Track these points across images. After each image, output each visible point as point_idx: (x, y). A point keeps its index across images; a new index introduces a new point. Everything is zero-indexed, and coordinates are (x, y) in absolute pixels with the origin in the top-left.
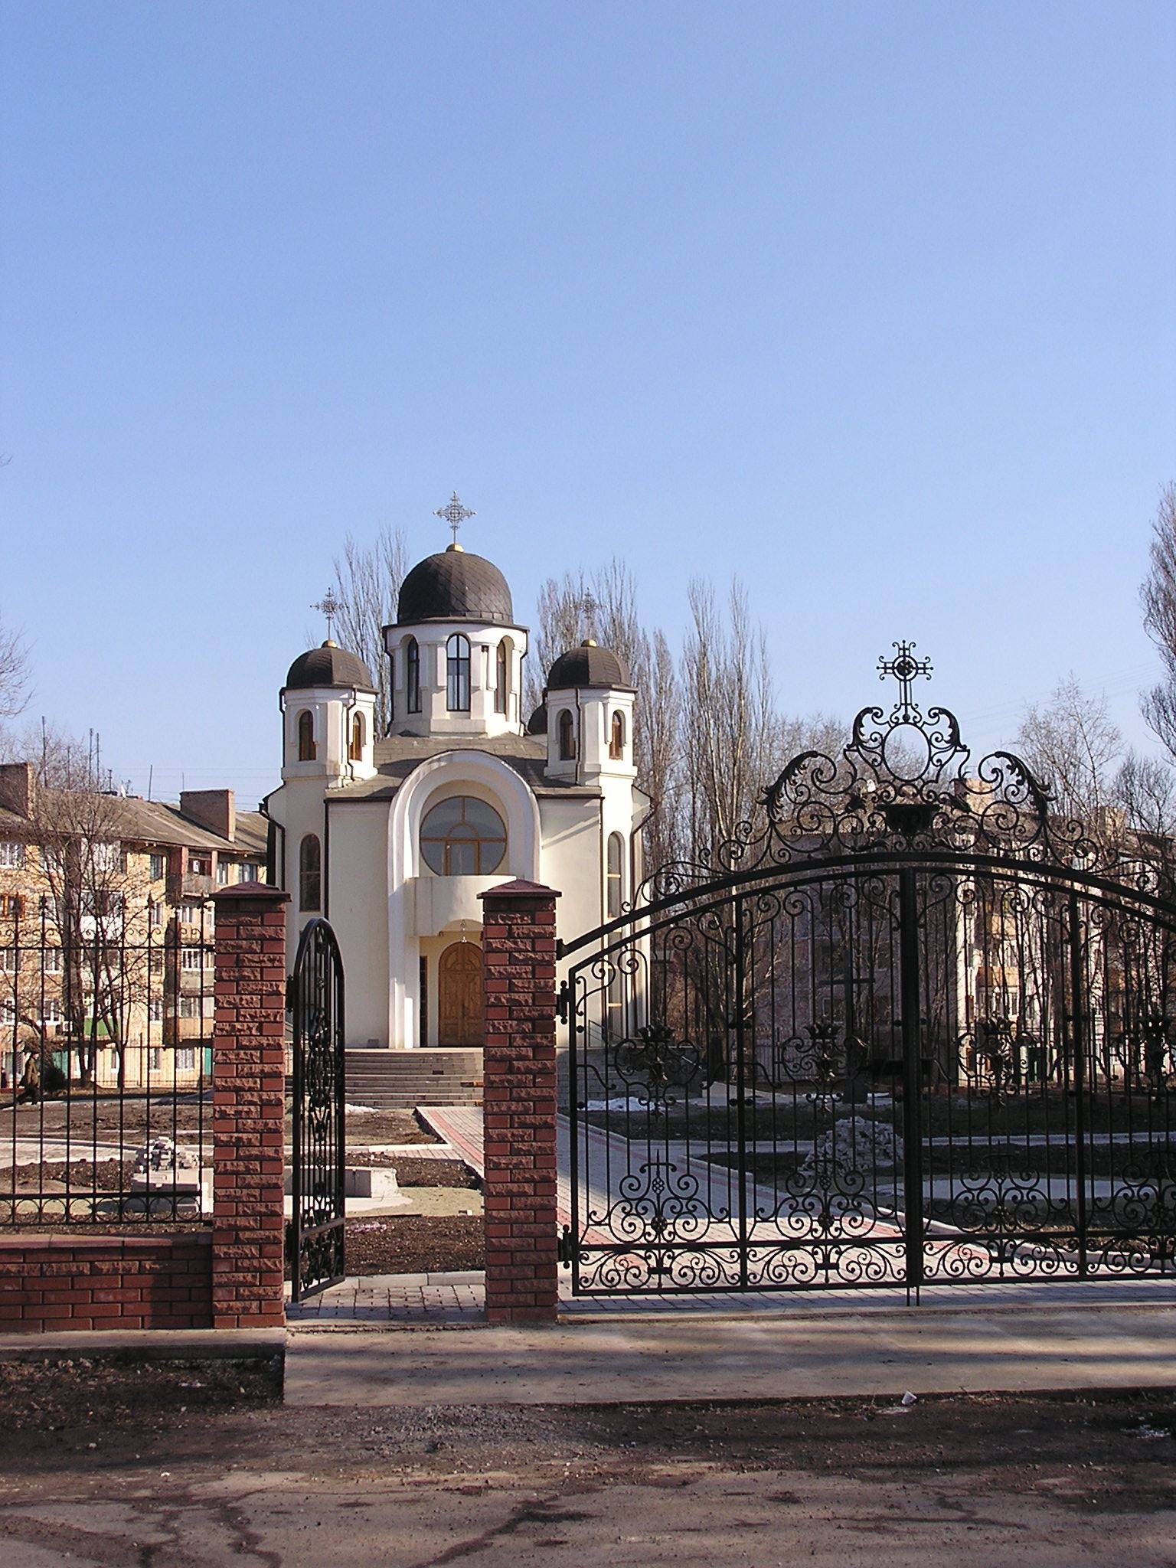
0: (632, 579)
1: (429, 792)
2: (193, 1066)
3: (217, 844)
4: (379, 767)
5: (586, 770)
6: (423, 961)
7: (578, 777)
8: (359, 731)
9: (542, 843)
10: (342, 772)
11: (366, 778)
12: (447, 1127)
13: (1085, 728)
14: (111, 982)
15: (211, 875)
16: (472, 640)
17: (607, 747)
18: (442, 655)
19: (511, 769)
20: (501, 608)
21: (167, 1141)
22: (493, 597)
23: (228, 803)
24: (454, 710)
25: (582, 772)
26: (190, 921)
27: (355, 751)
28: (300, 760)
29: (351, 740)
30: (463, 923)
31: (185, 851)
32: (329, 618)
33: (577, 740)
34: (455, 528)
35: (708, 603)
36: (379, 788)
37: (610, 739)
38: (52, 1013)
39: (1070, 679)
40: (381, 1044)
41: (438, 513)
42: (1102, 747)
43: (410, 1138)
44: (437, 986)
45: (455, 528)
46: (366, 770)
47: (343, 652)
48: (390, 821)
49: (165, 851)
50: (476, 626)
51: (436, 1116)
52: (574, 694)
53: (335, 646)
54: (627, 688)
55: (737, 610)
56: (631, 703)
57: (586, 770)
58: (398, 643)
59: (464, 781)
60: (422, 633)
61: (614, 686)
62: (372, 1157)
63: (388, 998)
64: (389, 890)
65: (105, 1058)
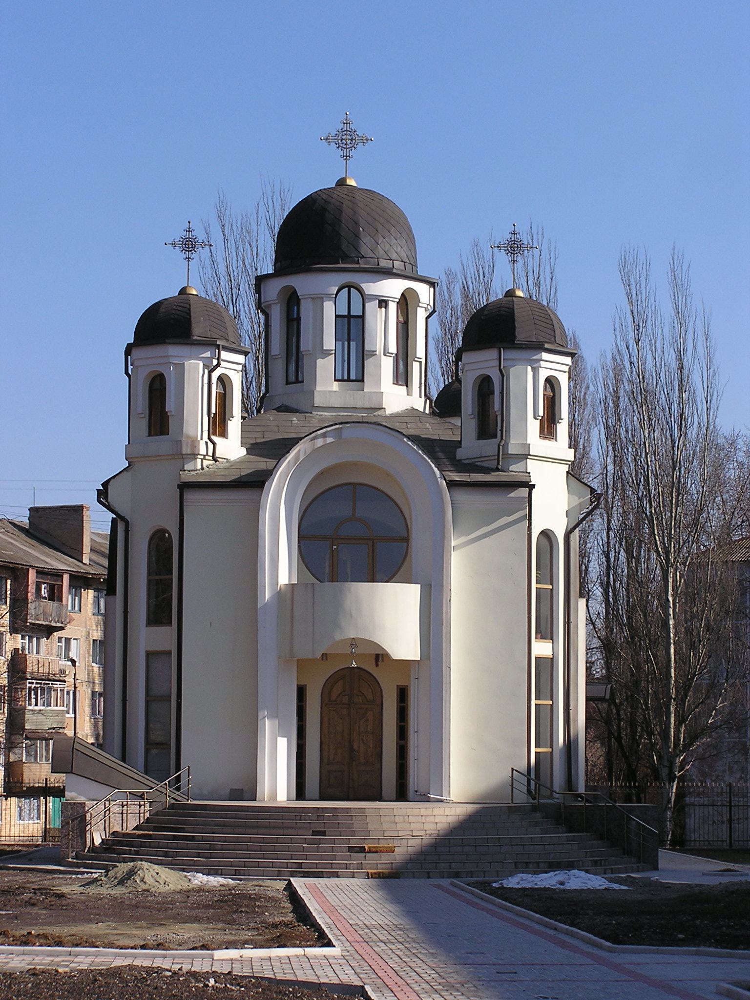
0: (552, 249)
3: (69, 565)
4: (248, 446)
6: (301, 692)
8: (224, 400)
10: (203, 451)
12: (331, 911)
18: (329, 310)
20: (403, 255)
25: (506, 455)
26: (38, 653)
27: (218, 425)
28: (150, 435)
29: (213, 410)
30: (354, 643)
34: (346, 157)
35: (643, 279)
45: (346, 157)
47: (210, 308)
51: (317, 893)
53: (194, 293)
55: (678, 287)
60: (304, 284)
61: (546, 346)
62: (212, 982)
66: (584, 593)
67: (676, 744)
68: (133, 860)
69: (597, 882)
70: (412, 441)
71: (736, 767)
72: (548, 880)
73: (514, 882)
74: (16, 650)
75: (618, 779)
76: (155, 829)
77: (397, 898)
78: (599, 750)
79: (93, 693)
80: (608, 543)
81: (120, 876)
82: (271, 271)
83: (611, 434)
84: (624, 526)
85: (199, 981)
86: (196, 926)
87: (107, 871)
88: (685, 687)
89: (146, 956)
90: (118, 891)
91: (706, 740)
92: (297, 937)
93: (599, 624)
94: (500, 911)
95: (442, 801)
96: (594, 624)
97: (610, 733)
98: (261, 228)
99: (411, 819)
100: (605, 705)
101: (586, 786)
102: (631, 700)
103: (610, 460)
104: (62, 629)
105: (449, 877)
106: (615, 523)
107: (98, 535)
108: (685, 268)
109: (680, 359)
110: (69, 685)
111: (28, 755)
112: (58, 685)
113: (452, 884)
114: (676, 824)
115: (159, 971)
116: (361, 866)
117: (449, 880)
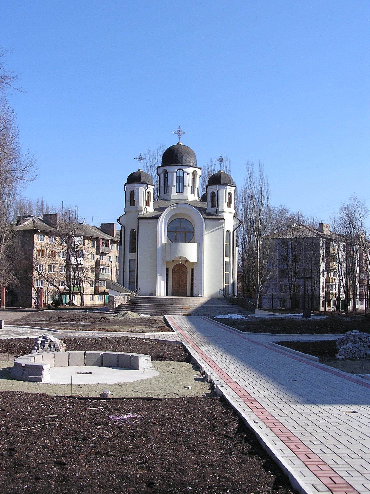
1: (169, 218)
2: (103, 300)
5: (219, 211)
6: (167, 269)
7: (217, 212)
8: (149, 197)
9: (205, 233)
10: (143, 210)
11: (151, 212)
12: (174, 323)
13: (359, 209)
14: (79, 275)
15: (108, 246)
16: (184, 171)
17: (226, 203)
18: (175, 175)
19: (196, 209)
21: (48, 335)
22: (191, 158)
23: (114, 227)
24: (178, 193)
25: (218, 211)
26: (103, 259)
27: (147, 203)
28: (130, 206)
29: (146, 200)
30: (180, 257)
32: (140, 162)
33: (217, 201)
34: (179, 137)
35: (252, 168)
36: (155, 215)
37: (227, 201)
38: (63, 284)
39: (354, 195)
40: (153, 295)
41: (175, 133)
42: (364, 214)
44: (171, 278)
45: (179, 137)
46: (151, 209)
48: (158, 225)
51: (171, 319)
52: (216, 187)
54: (232, 185)
55: (261, 170)
56: (234, 190)
57: (219, 211)
58: (161, 172)
59: (181, 213)
60: (169, 169)
61: (229, 185)
62: (145, 340)
63: (156, 281)
64: (157, 246)
65: (78, 297)
66: (237, 246)
68: (126, 311)
69: (240, 317)
72: (228, 316)
73: (219, 317)
74: (97, 259)
75: (245, 292)
77: (190, 320)
78: (240, 284)
79: (116, 269)
80: (243, 233)
83: (244, 207)
85: (142, 340)
86: (141, 327)
87: (119, 313)
88: (262, 269)
89: (128, 334)
91: (267, 282)
95: (202, 297)
96: (239, 253)
97: (243, 280)
100: (242, 273)
101: (237, 293)
102: (249, 272)
104: (109, 253)
107: (117, 230)
110: (110, 268)
112: (108, 268)
113: (204, 317)
114: (259, 303)
115: (132, 338)
116: (182, 312)
117: (203, 316)
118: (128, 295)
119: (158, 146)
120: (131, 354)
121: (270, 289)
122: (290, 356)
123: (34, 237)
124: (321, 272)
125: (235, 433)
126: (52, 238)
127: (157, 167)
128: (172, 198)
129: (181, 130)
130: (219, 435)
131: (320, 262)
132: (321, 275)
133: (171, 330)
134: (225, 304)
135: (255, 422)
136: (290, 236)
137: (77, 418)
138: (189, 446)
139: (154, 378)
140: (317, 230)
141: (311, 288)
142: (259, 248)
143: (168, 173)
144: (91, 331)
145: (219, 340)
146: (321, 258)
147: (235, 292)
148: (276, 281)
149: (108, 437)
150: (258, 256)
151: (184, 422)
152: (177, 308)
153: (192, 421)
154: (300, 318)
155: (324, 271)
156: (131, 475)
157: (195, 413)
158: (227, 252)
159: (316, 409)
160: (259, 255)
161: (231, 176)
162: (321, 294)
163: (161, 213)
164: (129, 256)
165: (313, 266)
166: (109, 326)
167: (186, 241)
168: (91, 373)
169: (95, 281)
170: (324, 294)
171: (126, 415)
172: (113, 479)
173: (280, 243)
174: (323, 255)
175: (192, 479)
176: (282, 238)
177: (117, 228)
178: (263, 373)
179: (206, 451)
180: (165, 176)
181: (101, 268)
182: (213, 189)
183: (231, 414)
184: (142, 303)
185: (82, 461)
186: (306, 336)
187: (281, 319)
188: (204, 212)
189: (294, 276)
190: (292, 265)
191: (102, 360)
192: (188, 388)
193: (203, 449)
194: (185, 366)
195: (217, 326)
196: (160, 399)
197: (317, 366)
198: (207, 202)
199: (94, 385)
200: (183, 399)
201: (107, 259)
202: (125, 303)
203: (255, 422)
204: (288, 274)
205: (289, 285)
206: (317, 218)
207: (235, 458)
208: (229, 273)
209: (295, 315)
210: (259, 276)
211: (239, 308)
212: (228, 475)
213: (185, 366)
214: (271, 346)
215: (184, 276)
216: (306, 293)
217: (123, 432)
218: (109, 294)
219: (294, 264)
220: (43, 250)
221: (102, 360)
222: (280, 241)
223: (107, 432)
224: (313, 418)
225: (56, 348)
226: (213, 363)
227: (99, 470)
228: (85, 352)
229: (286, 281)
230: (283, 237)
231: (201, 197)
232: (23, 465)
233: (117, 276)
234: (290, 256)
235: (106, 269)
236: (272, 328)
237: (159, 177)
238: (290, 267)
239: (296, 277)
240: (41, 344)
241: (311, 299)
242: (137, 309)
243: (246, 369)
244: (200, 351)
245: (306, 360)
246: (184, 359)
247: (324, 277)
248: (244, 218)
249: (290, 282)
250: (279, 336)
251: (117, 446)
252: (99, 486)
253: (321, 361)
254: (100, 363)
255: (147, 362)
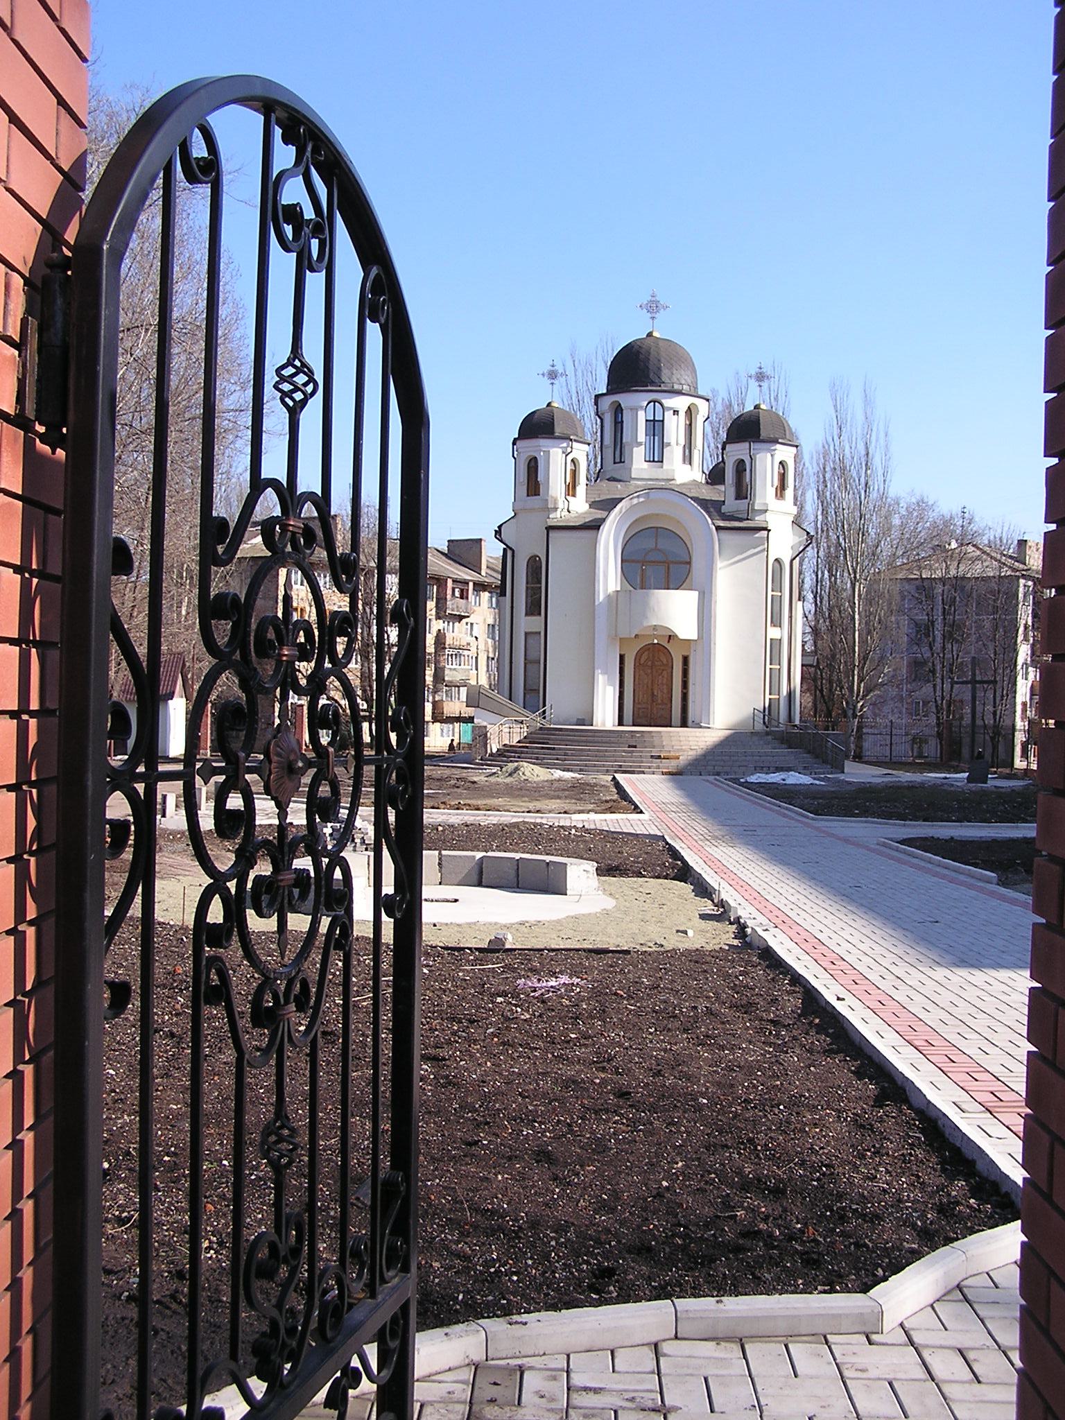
6: (622, 657)
7: (749, 514)
8: (574, 473)
10: (560, 505)
12: (641, 794)
15: (467, 598)
16: (665, 405)
19: (696, 505)
20: (689, 382)
22: (683, 372)
24: (650, 461)
25: (753, 509)
27: (571, 489)
28: (528, 495)
29: (568, 481)
30: (655, 628)
31: (450, 581)
32: (552, 384)
33: (749, 483)
34: (653, 318)
41: (641, 306)
43: (609, 805)
45: (653, 318)
46: (579, 506)
49: (436, 582)
50: (665, 394)
51: (632, 783)
55: (867, 401)
60: (625, 399)
61: (780, 441)
62: (573, 831)
66: (801, 598)
67: (858, 695)
68: (517, 761)
69: (806, 780)
70: (694, 501)
71: (896, 710)
72: (775, 778)
73: (753, 779)
74: (439, 630)
75: (820, 716)
76: (530, 743)
77: (681, 787)
78: (809, 698)
79: (488, 658)
80: (817, 566)
81: (509, 771)
82: (605, 391)
83: (821, 494)
84: (828, 555)
85: (565, 831)
86: (558, 801)
87: (502, 768)
88: (864, 659)
89: (531, 817)
90: (509, 780)
91: (877, 692)
92: (621, 808)
93: (810, 617)
94: (746, 796)
95: (709, 728)
96: (806, 617)
97: (816, 687)
98: (599, 363)
99: (690, 739)
100: (813, 669)
101: (800, 720)
102: (830, 666)
103: (819, 513)
104: (468, 617)
105: (713, 775)
106: (821, 554)
107: (491, 557)
108: (873, 390)
109: (867, 448)
110: (473, 653)
111: (447, 695)
112: (466, 653)
113: (715, 779)
114: (856, 746)
115: (541, 825)
116: (658, 767)
117: (713, 777)
118: (522, 722)
119: (601, 339)
120: (548, 858)
121: (886, 709)
122: (928, 871)
123: (278, 575)
124: (1019, 667)
125: (795, 1018)
126: (325, 577)
127: (596, 396)
128: (633, 476)
129: (658, 299)
130: (761, 1019)
131: (1016, 641)
132: (1021, 674)
133: (634, 809)
134: (770, 746)
135: (839, 999)
136: (940, 574)
137: (448, 983)
138: (697, 1038)
139: (606, 913)
140: (1011, 557)
141: (992, 709)
142: (859, 605)
143: (622, 410)
144: (438, 808)
145: (755, 833)
146: (1021, 630)
147: (795, 715)
148: (903, 690)
149: (522, 1017)
150: (855, 623)
151: (683, 994)
152: (646, 757)
153: (701, 993)
154: (959, 784)
155: (1026, 664)
156: (582, 1079)
157: (707, 979)
158: (774, 615)
159: (978, 976)
160: (857, 622)
161: (790, 422)
162: (1020, 724)
163: (607, 513)
164: (526, 623)
165: (998, 652)
166: (478, 798)
167: (671, 586)
168: (456, 901)
169: (434, 686)
170: (1026, 723)
171: (554, 979)
172: (545, 1084)
173: (913, 592)
174: (1027, 622)
175: (707, 1089)
176: (917, 579)
177: (492, 551)
178: (862, 905)
179: (734, 1045)
180: (616, 417)
181: (450, 653)
182: (741, 452)
183: (786, 982)
184: (556, 742)
185: (478, 1055)
186: (973, 826)
187: (912, 787)
188: (717, 512)
189: (950, 678)
190: (944, 648)
191: (481, 873)
192: (685, 932)
193: (728, 1042)
194: (676, 888)
195: (751, 801)
196: (627, 952)
197: (992, 894)
198: (724, 484)
199: (469, 924)
200: (676, 954)
201: (464, 630)
202: (515, 742)
203: (839, 999)
204: (933, 672)
205: (936, 701)
206: (1012, 527)
207: (796, 1059)
208: (778, 667)
209: (948, 776)
210: (856, 677)
211: (803, 757)
212: (782, 1084)
213: (676, 888)
214: (882, 848)
215: (666, 676)
216: (979, 722)
217: (553, 1010)
218: (475, 720)
219: (950, 647)
220: (301, 609)
221: (481, 873)
222: (914, 587)
223: (519, 1010)
224: (971, 994)
225: (367, 844)
226: (742, 883)
227: (517, 1070)
228: (440, 854)
229: (927, 689)
230: (921, 575)
231: (707, 473)
232: (359, 1059)
233: (490, 674)
234: (939, 625)
235: (462, 657)
236: (886, 807)
237: (599, 420)
238: (938, 654)
239: (952, 679)
240: (331, 835)
241: (992, 739)
242: (544, 758)
243: (821, 897)
244: (710, 857)
245: (968, 880)
246: (672, 875)
247: (1026, 679)
248: (819, 526)
249: (939, 693)
250: (904, 825)
251: (545, 1034)
252: (520, 1094)
253: (1003, 883)
254: (475, 878)
255: (588, 877)
